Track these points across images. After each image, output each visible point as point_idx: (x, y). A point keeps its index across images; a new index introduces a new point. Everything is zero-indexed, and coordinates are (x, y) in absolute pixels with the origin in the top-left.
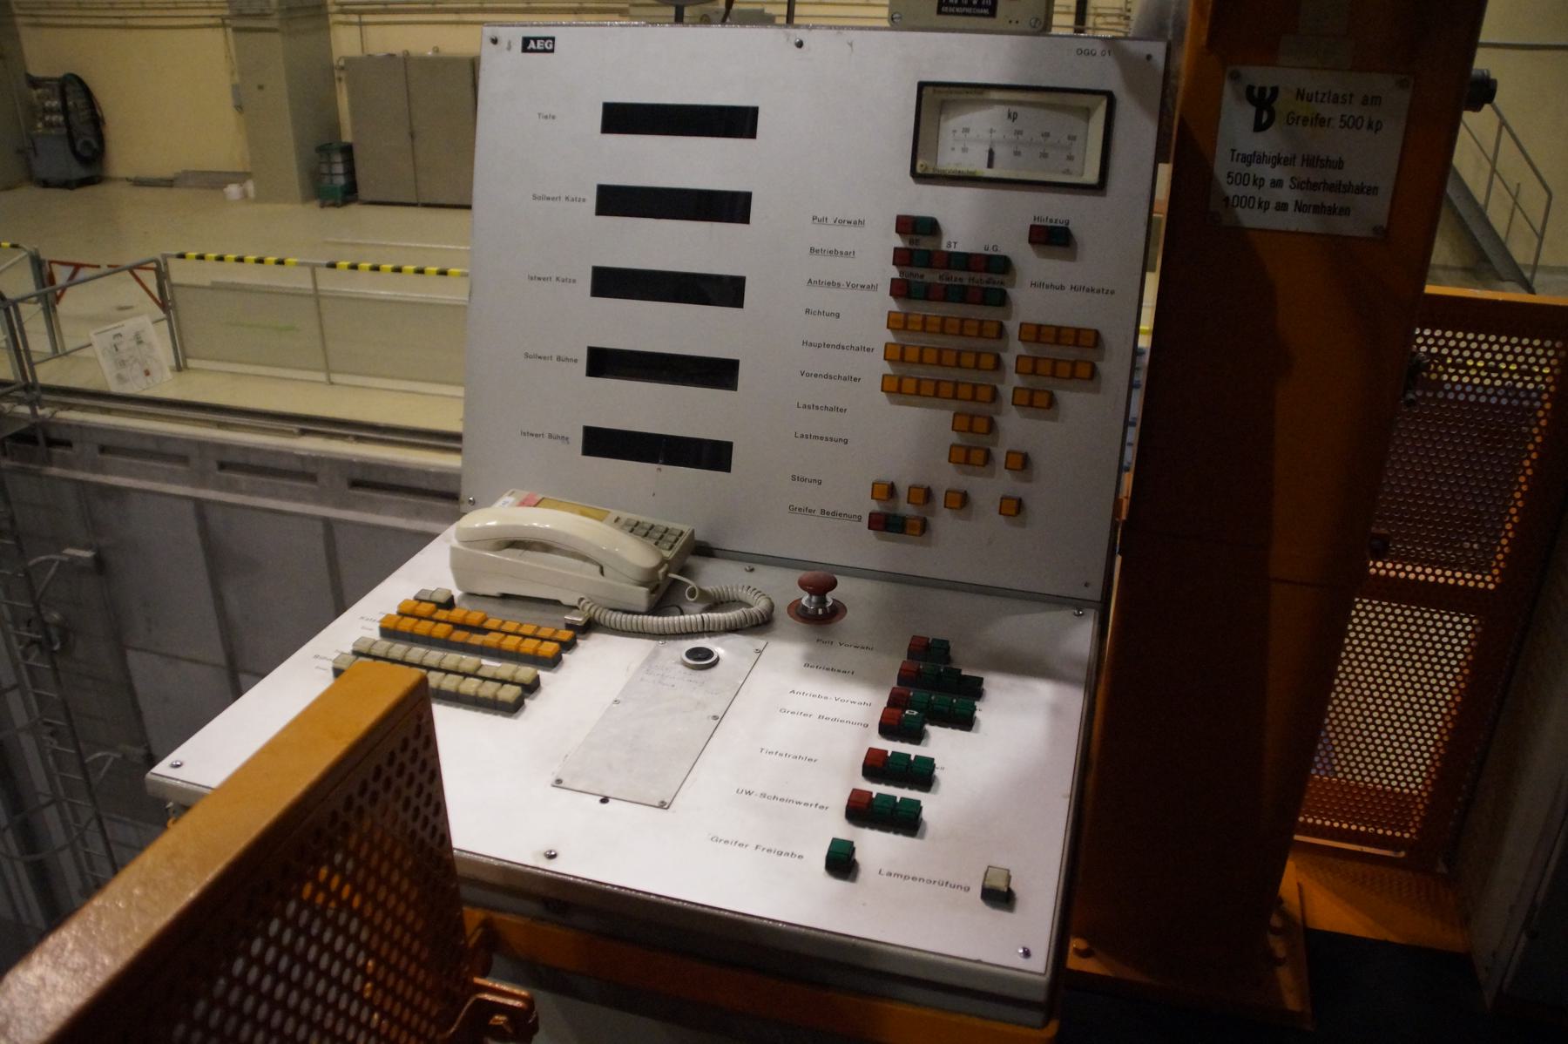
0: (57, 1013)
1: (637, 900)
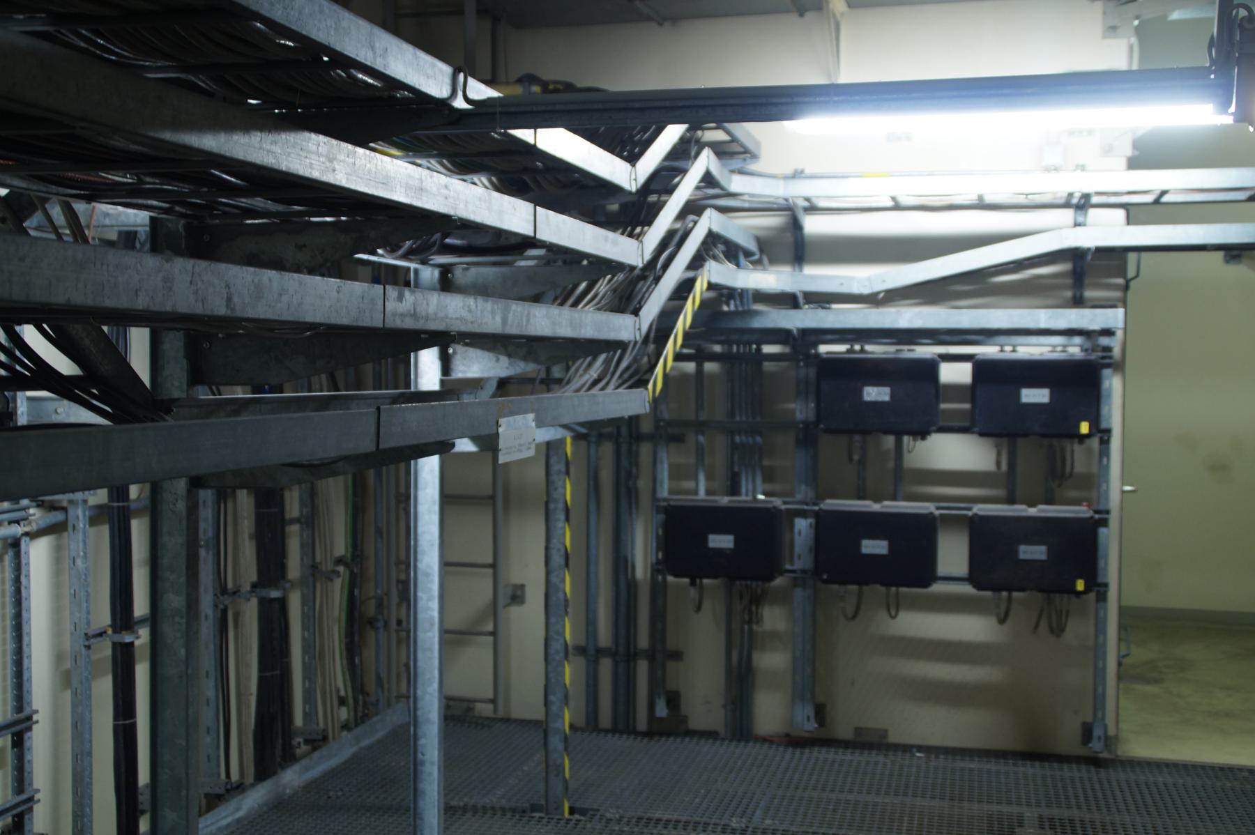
0: (1113, 29)
1: (779, 304)
